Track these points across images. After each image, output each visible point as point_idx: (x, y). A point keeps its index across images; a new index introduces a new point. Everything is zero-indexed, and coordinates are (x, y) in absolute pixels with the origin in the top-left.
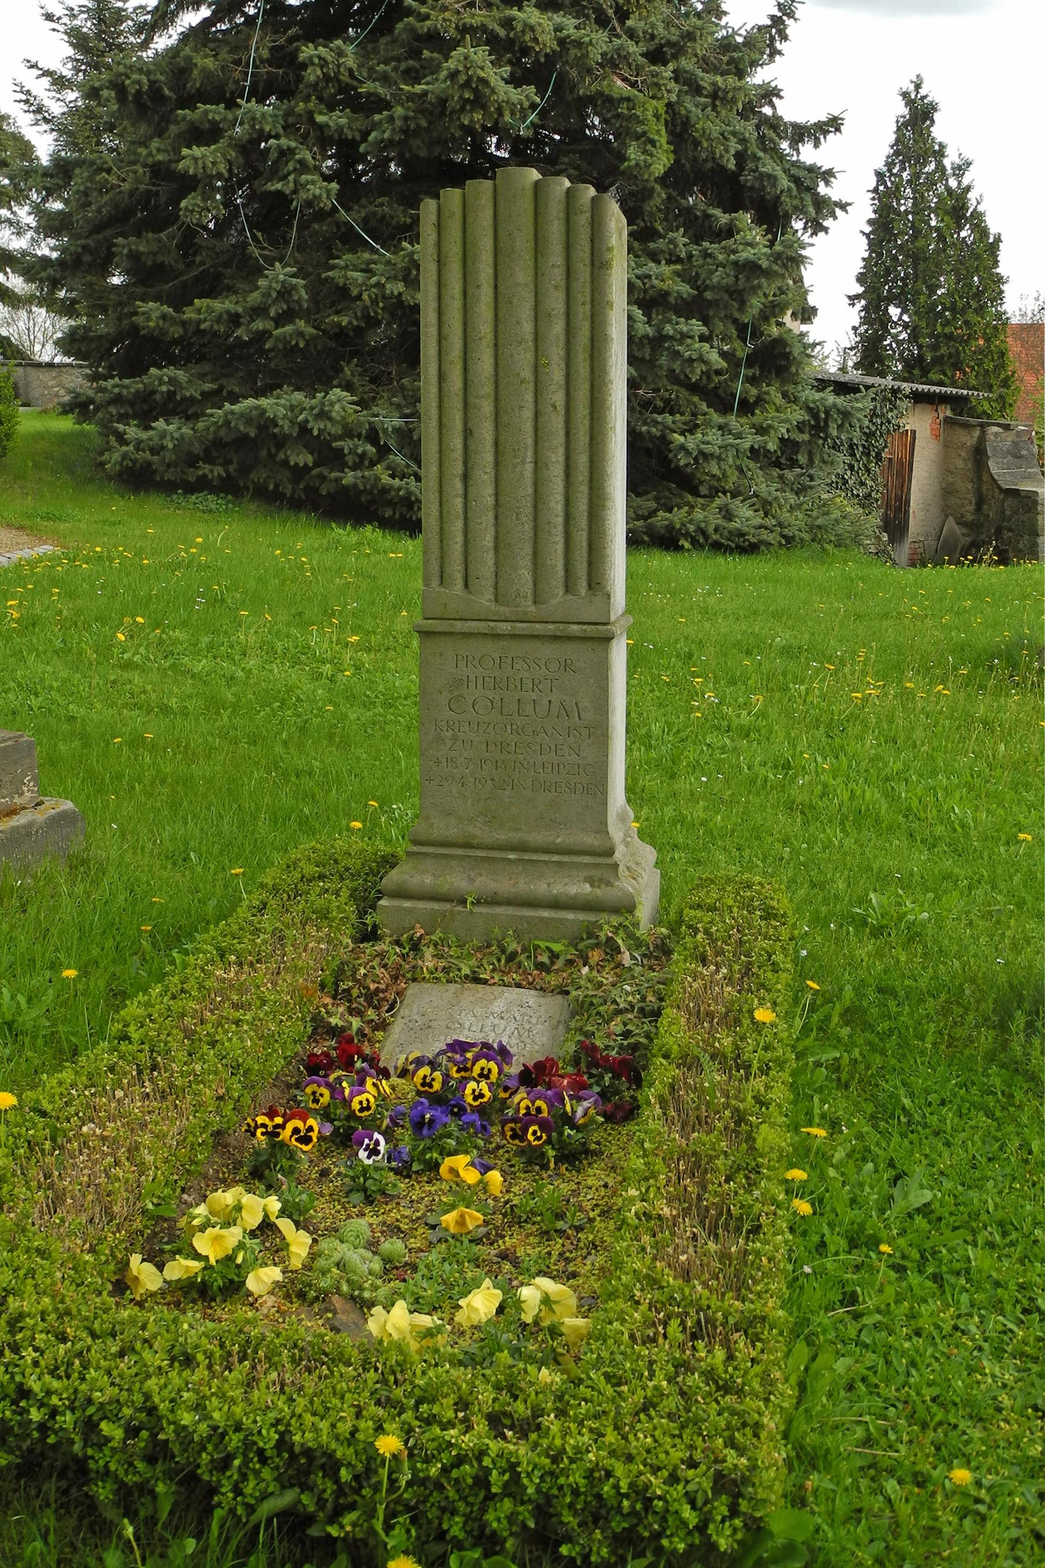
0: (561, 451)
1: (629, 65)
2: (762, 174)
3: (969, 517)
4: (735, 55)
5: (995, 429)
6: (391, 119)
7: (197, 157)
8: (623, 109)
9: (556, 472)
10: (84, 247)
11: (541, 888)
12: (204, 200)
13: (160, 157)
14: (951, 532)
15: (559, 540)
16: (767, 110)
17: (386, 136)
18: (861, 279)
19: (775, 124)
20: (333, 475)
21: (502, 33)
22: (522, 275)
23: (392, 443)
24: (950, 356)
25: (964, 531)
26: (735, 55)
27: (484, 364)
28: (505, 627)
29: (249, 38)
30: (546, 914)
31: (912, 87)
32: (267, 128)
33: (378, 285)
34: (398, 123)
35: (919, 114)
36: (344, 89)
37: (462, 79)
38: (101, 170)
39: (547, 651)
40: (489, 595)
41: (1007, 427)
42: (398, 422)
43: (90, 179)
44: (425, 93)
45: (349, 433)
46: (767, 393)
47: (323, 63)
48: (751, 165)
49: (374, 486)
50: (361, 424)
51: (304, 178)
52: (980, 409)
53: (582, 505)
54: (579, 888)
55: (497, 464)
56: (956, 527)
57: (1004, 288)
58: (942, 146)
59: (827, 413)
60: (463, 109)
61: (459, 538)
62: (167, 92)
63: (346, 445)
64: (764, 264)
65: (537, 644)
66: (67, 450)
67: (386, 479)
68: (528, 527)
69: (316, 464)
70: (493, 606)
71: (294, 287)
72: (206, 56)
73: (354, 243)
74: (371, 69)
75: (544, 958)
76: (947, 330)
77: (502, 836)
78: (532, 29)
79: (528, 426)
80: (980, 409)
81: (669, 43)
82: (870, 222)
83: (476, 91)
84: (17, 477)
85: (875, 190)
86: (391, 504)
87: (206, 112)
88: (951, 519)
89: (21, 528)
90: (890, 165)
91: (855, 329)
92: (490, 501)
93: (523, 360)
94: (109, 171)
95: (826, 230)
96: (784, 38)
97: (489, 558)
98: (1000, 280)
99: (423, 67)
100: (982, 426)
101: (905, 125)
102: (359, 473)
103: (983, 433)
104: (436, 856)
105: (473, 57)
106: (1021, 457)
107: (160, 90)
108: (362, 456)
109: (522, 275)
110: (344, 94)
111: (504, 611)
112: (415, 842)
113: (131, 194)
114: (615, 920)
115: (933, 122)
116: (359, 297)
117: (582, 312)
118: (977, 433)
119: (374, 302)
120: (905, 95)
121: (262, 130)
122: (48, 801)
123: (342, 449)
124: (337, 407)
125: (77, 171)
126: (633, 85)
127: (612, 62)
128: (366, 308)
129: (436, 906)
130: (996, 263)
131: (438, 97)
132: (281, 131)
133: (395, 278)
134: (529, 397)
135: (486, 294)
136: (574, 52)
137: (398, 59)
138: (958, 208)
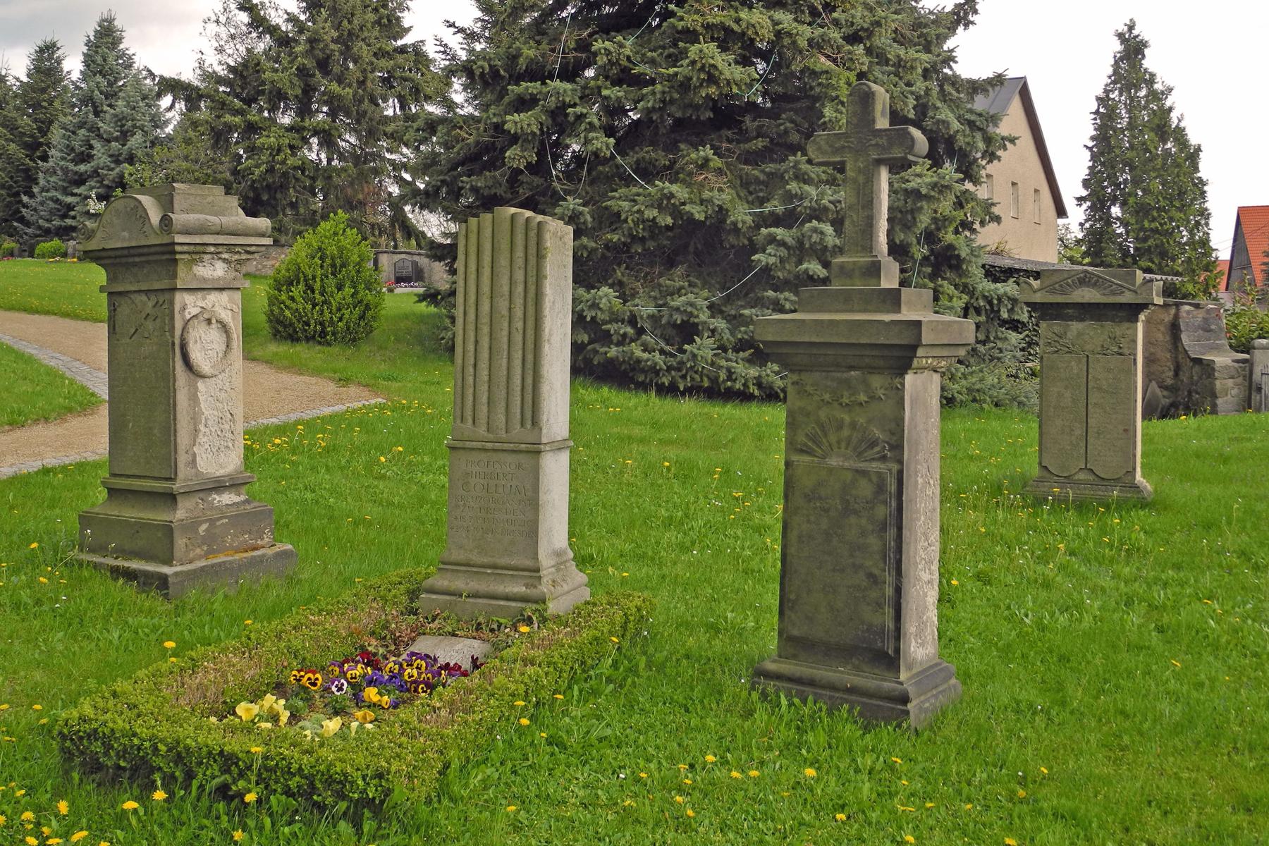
0: (520, 352)
1: (832, 46)
2: (938, 121)
3: (1169, 382)
4: (925, 31)
5: (1187, 308)
6: (654, 93)
7: (517, 121)
8: (823, 80)
9: (517, 363)
10: (443, 182)
11: (501, 588)
12: (522, 151)
13: (495, 120)
14: (1153, 393)
15: (519, 398)
16: (946, 70)
17: (650, 105)
18: (1086, 184)
19: (955, 81)
20: (603, 350)
21: (735, 27)
22: (503, 261)
23: (647, 326)
24: (1157, 246)
25: (1165, 393)
26: (925, 31)
27: (485, 307)
28: (489, 445)
29: (562, 33)
30: (502, 603)
31: (1126, 29)
32: (567, 100)
33: (639, 211)
34: (658, 96)
35: (1132, 48)
36: (625, 70)
37: (699, 65)
38: (455, 127)
39: (510, 458)
40: (484, 428)
41: (1197, 306)
42: (651, 310)
43: (448, 134)
44: (676, 74)
45: (615, 318)
46: (941, 286)
47: (608, 53)
48: (931, 114)
49: (630, 358)
50: (624, 312)
51: (591, 135)
52: (1184, 290)
53: (529, 380)
54: (519, 589)
55: (490, 359)
56: (1158, 391)
57: (1206, 188)
58: (1153, 75)
59: (999, 300)
60: (701, 85)
61: (471, 398)
62: (502, 72)
63: (612, 328)
64: (924, 191)
65: (506, 454)
66: (423, 327)
67: (638, 353)
68: (504, 392)
69: (590, 342)
70: (486, 434)
71: (581, 213)
72: (531, 48)
73: (628, 181)
74: (644, 55)
75: (495, 626)
76: (1153, 225)
77: (486, 560)
78: (753, 26)
79: (505, 339)
80: (1184, 290)
81: (862, 28)
82: (1092, 138)
83: (709, 73)
84: (380, 348)
85: (1097, 112)
86: (643, 371)
87: (527, 88)
88: (1154, 384)
89: (366, 386)
90: (1107, 92)
91: (1081, 225)
92: (486, 378)
93: (503, 305)
94: (461, 128)
95: (999, 158)
96: (976, 12)
97: (485, 409)
98: (1202, 183)
99: (681, 53)
100: (1177, 305)
101: (1121, 59)
102: (621, 349)
103: (1178, 310)
104: (453, 571)
105: (706, 50)
106: (1211, 331)
107: (498, 71)
108: (625, 335)
109: (503, 261)
110: (624, 76)
111: (491, 436)
112: (444, 563)
113: (477, 143)
114: (534, 606)
115: (1144, 57)
116: (626, 221)
117: (532, 280)
118: (1173, 311)
119: (636, 224)
120: (1120, 36)
121: (564, 102)
122: (278, 545)
123: (609, 331)
124: (604, 300)
125: (440, 128)
126: (834, 61)
127: (816, 45)
128: (630, 229)
129: (448, 598)
130: (1197, 169)
131: (685, 77)
132: (578, 101)
133: (652, 206)
134: (506, 324)
135: (486, 272)
136: (786, 41)
137: (664, 48)
138: (1163, 126)
